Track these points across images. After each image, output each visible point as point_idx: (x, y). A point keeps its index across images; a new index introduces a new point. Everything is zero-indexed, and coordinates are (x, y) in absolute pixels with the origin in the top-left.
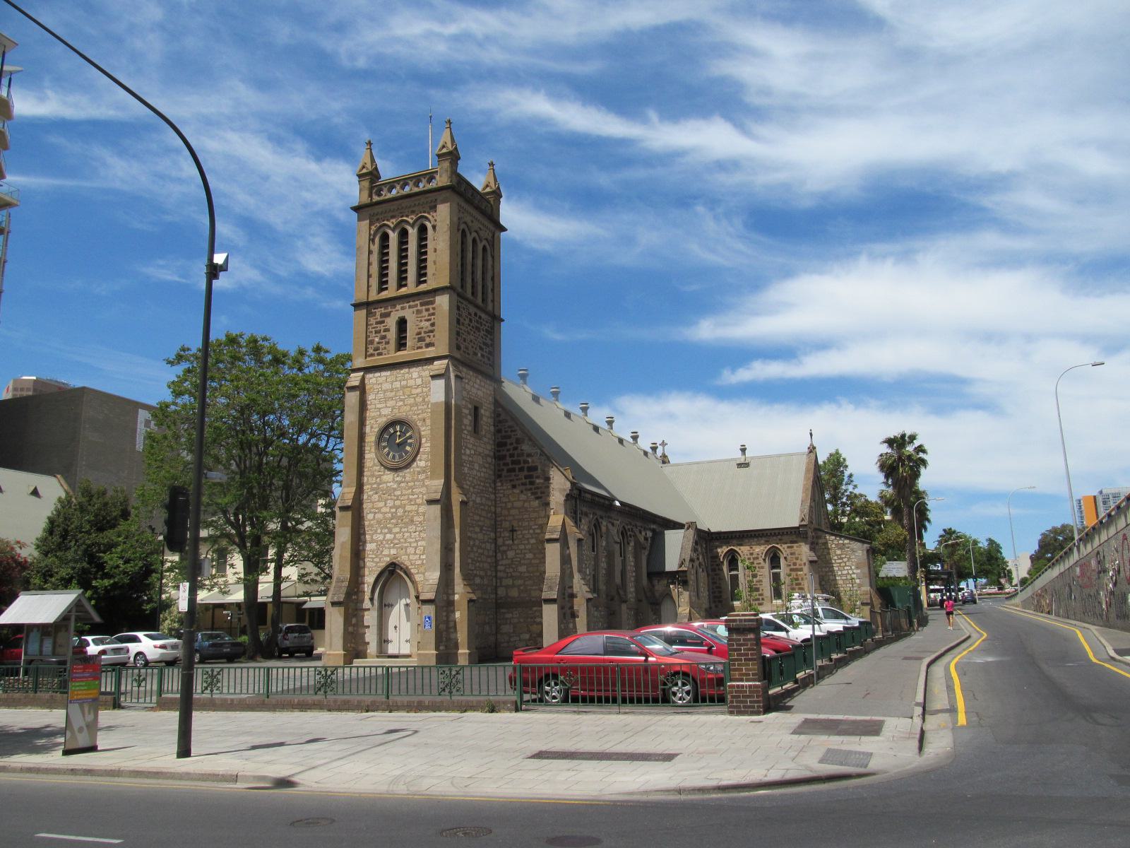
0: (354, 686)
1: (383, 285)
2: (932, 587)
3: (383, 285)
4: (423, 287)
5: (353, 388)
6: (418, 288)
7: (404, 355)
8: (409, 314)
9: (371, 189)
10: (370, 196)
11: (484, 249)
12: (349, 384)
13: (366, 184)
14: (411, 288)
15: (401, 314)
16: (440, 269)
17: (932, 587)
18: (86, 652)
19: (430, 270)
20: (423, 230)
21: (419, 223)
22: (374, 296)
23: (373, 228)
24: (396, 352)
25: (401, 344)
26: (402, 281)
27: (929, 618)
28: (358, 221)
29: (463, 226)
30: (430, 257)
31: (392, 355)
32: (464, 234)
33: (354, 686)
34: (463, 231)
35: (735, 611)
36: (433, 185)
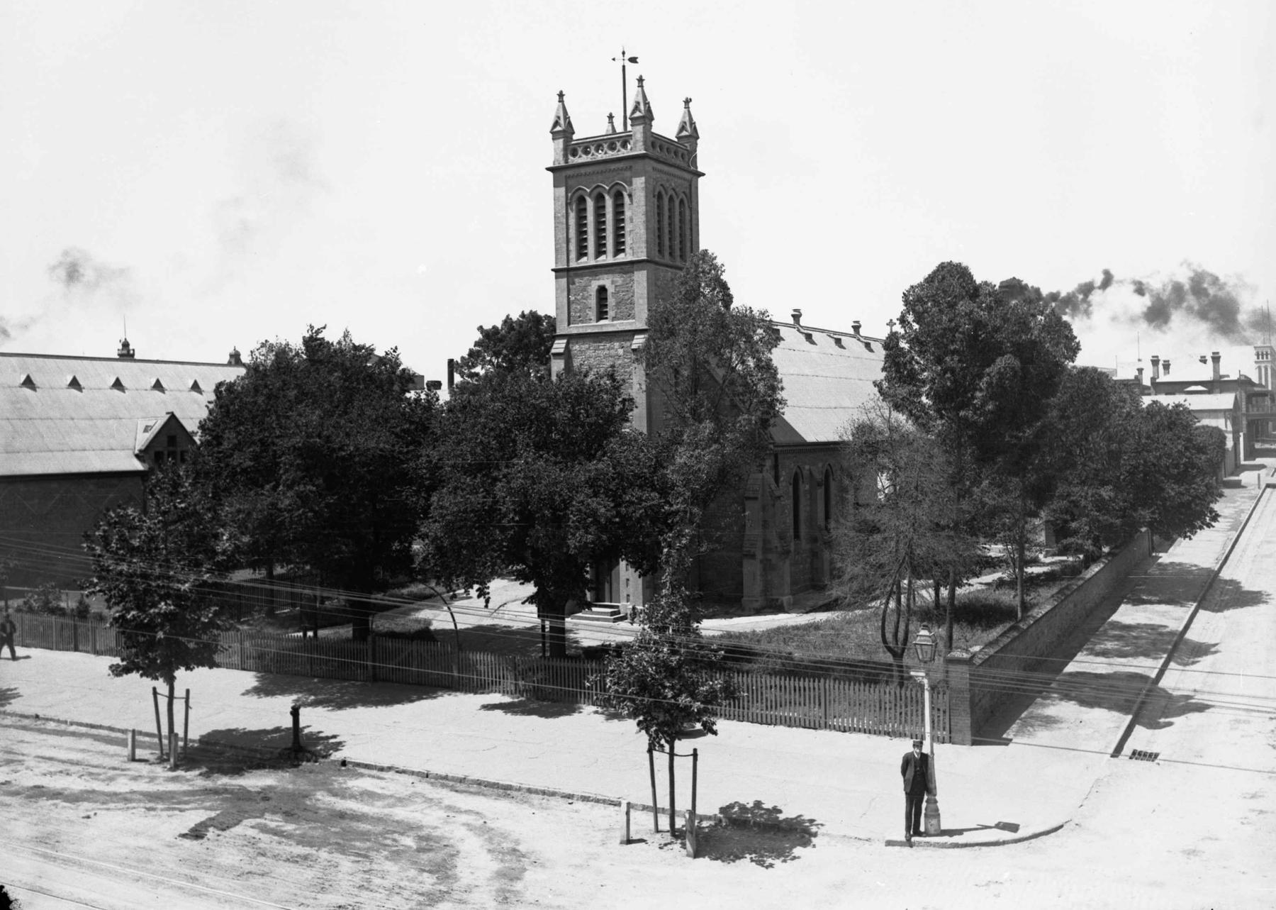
0: (774, 720)
1: (582, 252)
2: (1258, 446)
3: (582, 252)
4: (621, 258)
5: (557, 355)
6: (618, 257)
7: (607, 325)
8: (606, 281)
9: (565, 149)
10: (565, 156)
11: (682, 202)
12: (553, 351)
13: (561, 142)
14: (608, 258)
15: (601, 283)
16: (637, 246)
17: (1258, 446)
18: (178, 668)
19: (628, 240)
20: (618, 197)
21: (614, 191)
22: (573, 264)
23: (570, 195)
24: (598, 321)
25: (602, 315)
26: (600, 251)
27: (536, 616)
28: (554, 186)
29: (659, 188)
30: (628, 227)
31: (593, 326)
32: (660, 197)
33: (774, 720)
34: (660, 194)
35: (604, 601)
36: (623, 153)
